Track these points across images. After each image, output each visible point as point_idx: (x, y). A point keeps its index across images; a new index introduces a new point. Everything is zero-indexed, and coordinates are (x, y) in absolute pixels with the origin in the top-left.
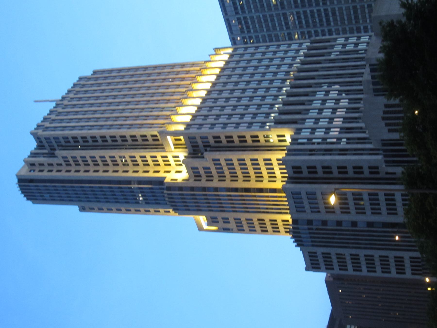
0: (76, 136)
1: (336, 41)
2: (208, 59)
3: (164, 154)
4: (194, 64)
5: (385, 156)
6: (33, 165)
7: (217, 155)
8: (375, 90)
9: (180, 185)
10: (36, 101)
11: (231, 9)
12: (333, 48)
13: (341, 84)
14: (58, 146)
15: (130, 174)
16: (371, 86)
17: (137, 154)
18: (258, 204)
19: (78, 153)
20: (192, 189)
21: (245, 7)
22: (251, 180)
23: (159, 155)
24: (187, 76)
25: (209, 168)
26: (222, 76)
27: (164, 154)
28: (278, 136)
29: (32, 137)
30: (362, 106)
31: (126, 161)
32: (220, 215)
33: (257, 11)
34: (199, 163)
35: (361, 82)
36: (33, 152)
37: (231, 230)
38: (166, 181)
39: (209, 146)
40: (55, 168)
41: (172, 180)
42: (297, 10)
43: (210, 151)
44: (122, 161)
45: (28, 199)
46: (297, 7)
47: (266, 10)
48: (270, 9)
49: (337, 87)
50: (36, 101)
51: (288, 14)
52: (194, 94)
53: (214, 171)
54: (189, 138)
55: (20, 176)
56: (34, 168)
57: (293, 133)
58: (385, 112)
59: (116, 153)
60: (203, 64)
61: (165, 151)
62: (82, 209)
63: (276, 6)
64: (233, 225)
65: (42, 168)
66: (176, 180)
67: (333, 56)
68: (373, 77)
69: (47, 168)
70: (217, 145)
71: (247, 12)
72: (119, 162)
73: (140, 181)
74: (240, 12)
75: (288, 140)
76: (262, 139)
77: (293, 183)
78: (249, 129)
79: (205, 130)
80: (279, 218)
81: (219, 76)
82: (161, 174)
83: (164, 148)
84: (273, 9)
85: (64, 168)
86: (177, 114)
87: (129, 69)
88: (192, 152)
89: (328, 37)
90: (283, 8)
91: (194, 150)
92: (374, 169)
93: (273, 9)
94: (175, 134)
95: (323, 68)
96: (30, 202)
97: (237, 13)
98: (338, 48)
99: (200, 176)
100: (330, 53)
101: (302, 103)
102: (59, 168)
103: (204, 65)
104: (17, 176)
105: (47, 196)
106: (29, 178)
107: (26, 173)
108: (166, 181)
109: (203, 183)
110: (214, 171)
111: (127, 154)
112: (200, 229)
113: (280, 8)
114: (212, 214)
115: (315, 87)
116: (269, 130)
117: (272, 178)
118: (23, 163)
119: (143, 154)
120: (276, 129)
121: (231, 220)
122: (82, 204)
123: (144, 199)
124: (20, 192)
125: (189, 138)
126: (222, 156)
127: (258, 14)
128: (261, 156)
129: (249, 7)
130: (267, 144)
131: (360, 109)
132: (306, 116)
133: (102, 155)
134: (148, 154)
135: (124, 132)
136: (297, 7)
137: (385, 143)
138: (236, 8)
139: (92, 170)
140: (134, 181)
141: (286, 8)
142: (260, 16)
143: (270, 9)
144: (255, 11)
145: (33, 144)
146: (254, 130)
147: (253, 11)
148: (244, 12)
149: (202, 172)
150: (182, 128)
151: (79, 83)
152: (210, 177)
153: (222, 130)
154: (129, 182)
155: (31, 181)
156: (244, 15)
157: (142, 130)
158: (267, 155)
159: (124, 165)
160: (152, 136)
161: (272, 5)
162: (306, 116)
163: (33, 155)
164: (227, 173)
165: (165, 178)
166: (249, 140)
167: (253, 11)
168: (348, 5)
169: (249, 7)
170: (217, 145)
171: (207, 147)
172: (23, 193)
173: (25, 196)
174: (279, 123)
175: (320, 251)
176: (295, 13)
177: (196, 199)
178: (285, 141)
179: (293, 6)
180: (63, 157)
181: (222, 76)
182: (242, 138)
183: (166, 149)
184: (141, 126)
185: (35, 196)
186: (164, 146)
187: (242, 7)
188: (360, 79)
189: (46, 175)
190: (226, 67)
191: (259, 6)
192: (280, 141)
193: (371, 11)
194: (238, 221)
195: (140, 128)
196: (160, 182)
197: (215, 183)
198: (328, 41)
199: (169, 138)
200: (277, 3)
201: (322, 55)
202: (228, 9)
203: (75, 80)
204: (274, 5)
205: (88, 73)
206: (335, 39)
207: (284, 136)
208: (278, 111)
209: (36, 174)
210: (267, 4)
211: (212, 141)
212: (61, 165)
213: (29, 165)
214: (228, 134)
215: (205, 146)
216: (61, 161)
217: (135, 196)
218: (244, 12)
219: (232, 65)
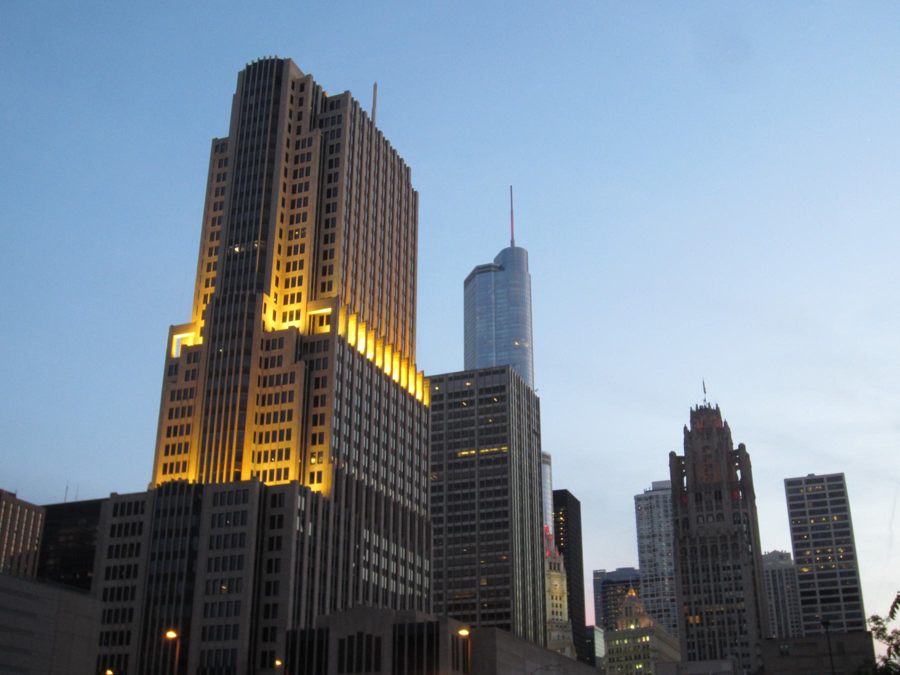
0: (341, 164)
1: (426, 558)
2: (419, 371)
3: (304, 297)
4: (412, 347)
5: (303, 633)
6: (302, 88)
7: (299, 380)
8: (402, 627)
9: (256, 317)
10: (375, 86)
11: (456, 387)
12: (385, 537)
13: (313, 538)
14: (326, 133)
15: (277, 241)
16: (407, 622)
17: (306, 257)
18: (218, 431)
19: (314, 164)
20: (250, 334)
21: (458, 410)
22: (257, 426)
23: (303, 289)
24: (400, 337)
25: (280, 365)
26: (353, 356)
27: (304, 297)
28: (320, 474)
29: (342, 92)
30: (380, 607)
31: (297, 237)
32: (202, 367)
33: (450, 426)
34: (289, 350)
35: (413, 608)
36: (320, 90)
37: (173, 377)
38: (265, 296)
39: (311, 369)
40: (294, 122)
41: (265, 305)
42: (445, 488)
43: (306, 370)
44: (298, 230)
45: (248, 67)
46: (450, 487)
47: (451, 441)
48: (450, 447)
49: (310, 532)
50: (375, 86)
51: (441, 473)
52: (371, 343)
53: (274, 371)
54: (326, 341)
55: (289, 66)
56: (297, 88)
57: (324, 496)
58: (369, 637)
59: (310, 224)
60: (363, 318)
61: (308, 301)
62: (219, 146)
63: (455, 456)
64: (182, 384)
65: (296, 102)
66: (265, 312)
67: (365, 534)
68: (421, 625)
69: (296, 110)
70: (313, 381)
71: (451, 411)
72: (295, 226)
73: (265, 254)
74: (451, 401)
75: (315, 487)
76: (317, 448)
77: (260, 493)
78: (332, 432)
79: (337, 366)
80: (193, 459)
81: (397, 385)
82: (273, 289)
83: (311, 300)
84: (451, 451)
85: (294, 138)
86: (358, 322)
87: (414, 248)
88: (304, 341)
89: (433, 548)
90: (450, 466)
91: (306, 345)
92: (272, 611)
93: (451, 451)
94: (332, 320)
95: (360, 520)
96: (243, 67)
97: (450, 396)
98: (375, 541)
99: (268, 349)
100: (368, 527)
101: (395, 530)
102: (294, 130)
103: (370, 328)
104: (289, 60)
105: (252, 100)
106: (283, 79)
107: (292, 75)
108: (265, 296)
109: (258, 353)
110: (274, 371)
111: (308, 241)
112: (174, 330)
113: (451, 461)
114: (204, 356)
115: (346, 513)
116: (330, 462)
117: (259, 458)
118: (306, 73)
119: (306, 265)
120: (330, 472)
121: (191, 384)
122: (230, 153)
123: (235, 254)
124: (262, 58)
125: (326, 341)
126: (297, 387)
127: (445, 427)
128: (293, 444)
129: (457, 415)
130: (308, 455)
131: (367, 601)
132: (382, 535)
133: (310, 202)
134: (305, 273)
135: (340, 241)
136: (450, 487)
137: (323, 633)
138: (457, 395)
139: (287, 181)
140: (266, 244)
141: (450, 472)
142: (442, 429)
143: (450, 447)
144: (450, 424)
145: (331, 90)
146: (331, 440)
147: (451, 421)
148: (450, 406)
149: (275, 353)
150: (341, 331)
151: (358, 111)
152: (266, 363)
153: (334, 392)
154: (266, 237)
155: (279, 81)
156: (445, 406)
157: (341, 270)
158: (294, 455)
159: (291, 233)
160: (330, 284)
161: (457, 450)
162: (382, 535)
163: (317, 89)
164: (270, 390)
165: (269, 295)
166: (318, 429)
167: (451, 421)
168: (444, 565)
169: (457, 415)
170: (313, 381)
171: (311, 366)
172: (260, 62)
173: (254, 64)
174: (337, 474)
175: (146, 519)
176: (441, 483)
177: (234, 337)
178: (312, 482)
179: (451, 482)
180: (310, 140)
181: (353, 356)
182: (318, 420)
183: (311, 304)
184: (345, 267)
185: (253, 80)
186: (313, 302)
187: (459, 405)
188: (416, 608)
189: (287, 106)
190: (374, 369)
191: (457, 430)
192: (312, 475)
193: (501, 626)
194: (189, 394)
195: (343, 267)
196: (263, 287)
197: (256, 371)
198: (428, 547)
199: (328, 311)
200: (459, 458)
201: (367, 516)
202: (458, 382)
203: (408, 162)
204: (456, 454)
205: (415, 184)
206: (429, 558)
207: (319, 481)
208: (350, 474)
209: (288, 92)
210: (459, 443)
211: (318, 374)
212: (299, 132)
213: (302, 82)
214: (328, 400)
215: (311, 362)
216: (305, 134)
217: (243, 241)
218: (450, 406)
219: (357, 365)
